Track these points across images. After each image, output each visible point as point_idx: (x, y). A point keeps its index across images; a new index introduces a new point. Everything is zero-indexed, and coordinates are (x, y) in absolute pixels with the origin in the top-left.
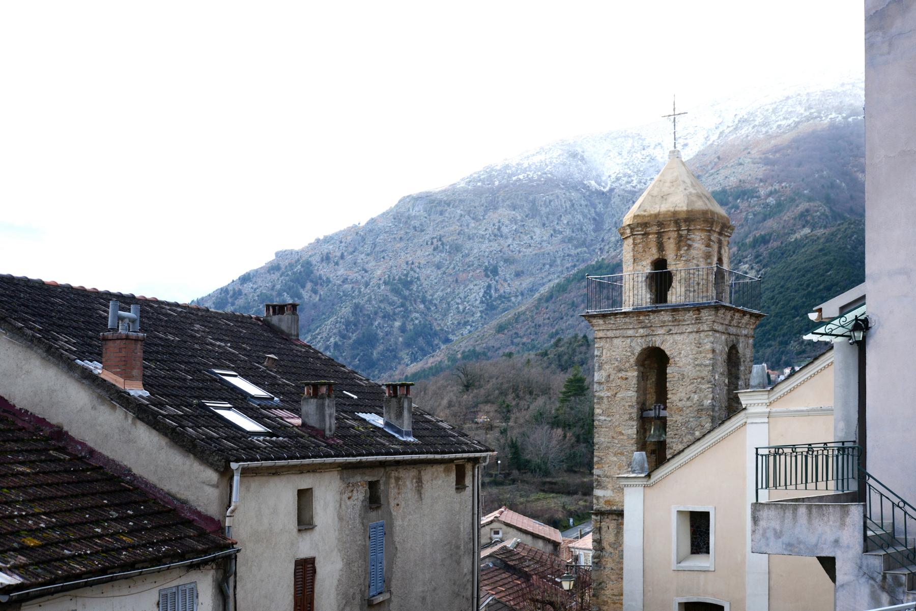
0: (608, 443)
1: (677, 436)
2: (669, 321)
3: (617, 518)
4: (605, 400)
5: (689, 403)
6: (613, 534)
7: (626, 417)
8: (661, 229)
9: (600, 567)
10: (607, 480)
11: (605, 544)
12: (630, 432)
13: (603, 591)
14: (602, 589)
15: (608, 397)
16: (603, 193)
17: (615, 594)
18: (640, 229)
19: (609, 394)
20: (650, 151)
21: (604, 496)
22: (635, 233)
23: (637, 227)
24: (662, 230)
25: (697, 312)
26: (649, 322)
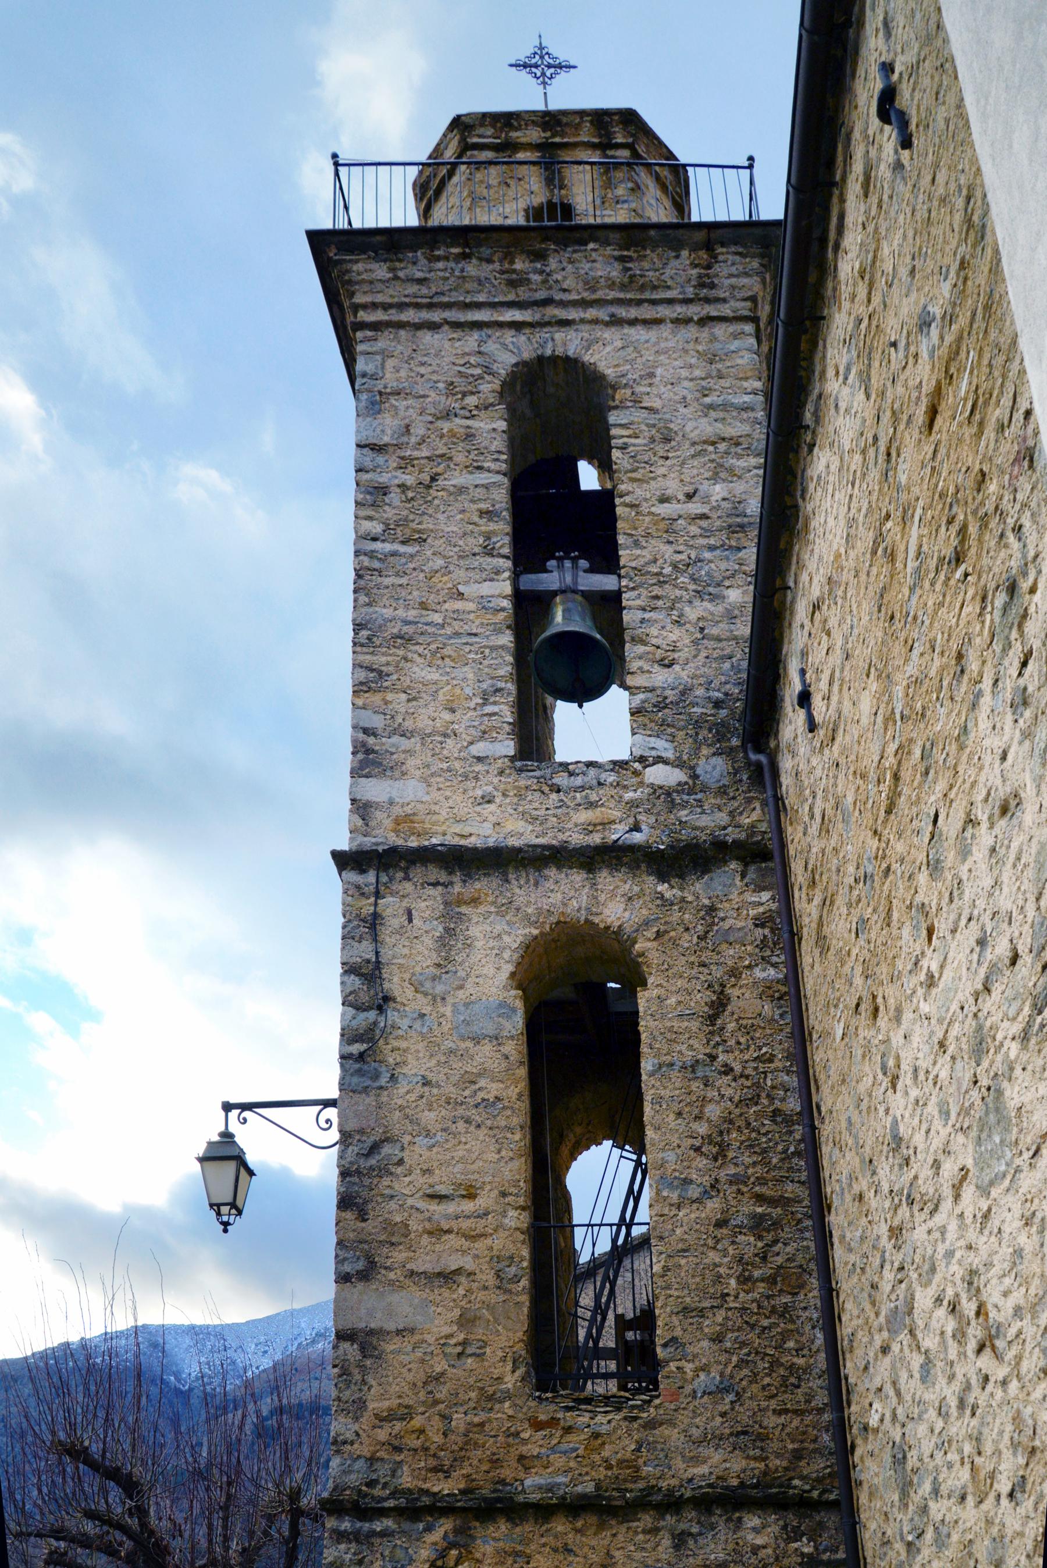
0: (407, 623)
1: (660, 603)
2: (612, 286)
3: (443, 877)
4: (395, 497)
5: (695, 508)
6: (428, 941)
7: (475, 543)
8: (553, 136)
9: (376, 1076)
10: (405, 744)
11: (395, 983)
12: (487, 589)
13: (386, 1181)
14: (383, 1171)
15: (402, 486)
16: (182, 1392)
17: (442, 1190)
18: (490, 131)
19: (410, 480)
20: (230, 1353)
21: (391, 802)
22: (475, 140)
23: (482, 125)
24: (557, 140)
25: (703, 254)
26: (545, 282)
